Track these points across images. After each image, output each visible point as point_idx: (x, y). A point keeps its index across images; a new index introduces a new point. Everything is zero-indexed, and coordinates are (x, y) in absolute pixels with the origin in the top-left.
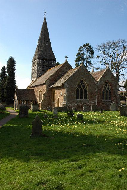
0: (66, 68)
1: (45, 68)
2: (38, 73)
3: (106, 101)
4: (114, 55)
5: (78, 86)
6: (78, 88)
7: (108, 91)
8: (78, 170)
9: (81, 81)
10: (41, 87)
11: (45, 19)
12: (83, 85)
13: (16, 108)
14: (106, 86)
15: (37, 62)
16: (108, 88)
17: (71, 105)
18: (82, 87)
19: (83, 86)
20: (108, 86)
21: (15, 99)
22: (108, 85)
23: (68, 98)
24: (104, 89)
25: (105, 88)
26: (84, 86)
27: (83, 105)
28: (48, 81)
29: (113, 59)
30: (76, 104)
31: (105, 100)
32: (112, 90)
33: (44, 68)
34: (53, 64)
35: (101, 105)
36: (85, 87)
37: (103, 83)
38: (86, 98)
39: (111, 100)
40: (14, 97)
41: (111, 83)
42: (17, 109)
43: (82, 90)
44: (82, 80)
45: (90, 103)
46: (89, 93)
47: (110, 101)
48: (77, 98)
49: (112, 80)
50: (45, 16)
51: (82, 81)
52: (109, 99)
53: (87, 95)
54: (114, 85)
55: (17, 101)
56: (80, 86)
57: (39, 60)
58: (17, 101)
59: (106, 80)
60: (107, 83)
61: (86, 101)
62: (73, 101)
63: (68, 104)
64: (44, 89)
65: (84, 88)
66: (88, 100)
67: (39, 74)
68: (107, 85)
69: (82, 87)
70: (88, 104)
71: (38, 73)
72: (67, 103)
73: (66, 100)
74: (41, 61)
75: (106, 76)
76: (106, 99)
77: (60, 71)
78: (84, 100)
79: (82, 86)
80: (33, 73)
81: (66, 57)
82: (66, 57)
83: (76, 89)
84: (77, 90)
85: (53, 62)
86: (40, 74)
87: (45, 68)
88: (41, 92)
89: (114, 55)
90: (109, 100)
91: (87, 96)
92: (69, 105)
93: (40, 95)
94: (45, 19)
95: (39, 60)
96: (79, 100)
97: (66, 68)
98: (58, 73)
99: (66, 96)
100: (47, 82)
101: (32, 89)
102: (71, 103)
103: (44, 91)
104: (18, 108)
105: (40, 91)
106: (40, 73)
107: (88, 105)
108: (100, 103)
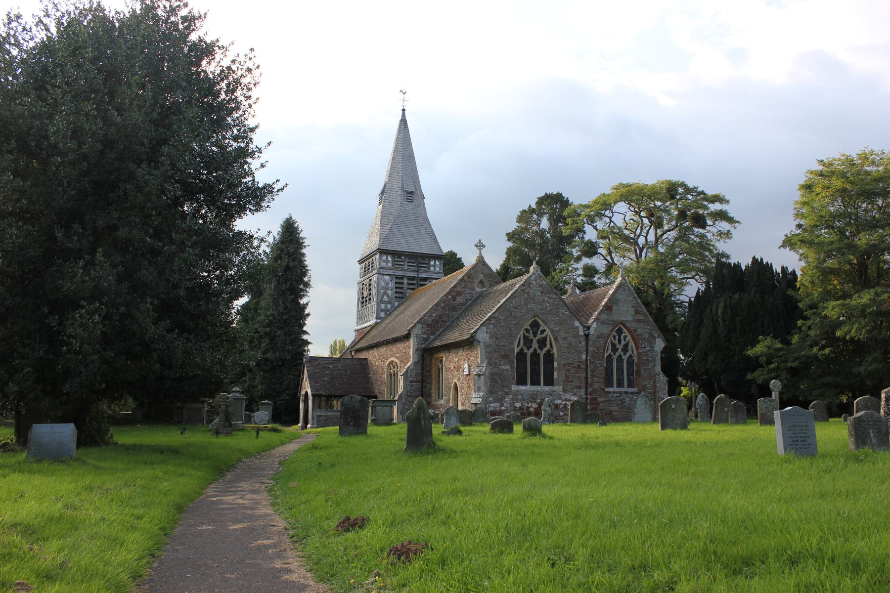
0: (481, 282)
1: (405, 286)
2: (380, 301)
3: (620, 393)
4: (646, 238)
5: (522, 342)
6: (522, 350)
7: (625, 358)
8: (785, 465)
9: (531, 325)
10: (394, 348)
11: (404, 122)
12: (539, 336)
13: (306, 422)
14: (617, 342)
15: (376, 264)
16: (625, 349)
17: (502, 405)
18: (535, 345)
19: (538, 341)
20: (623, 342)
21: (303, 393)
22: (625, 337)
23: (495, 383)
24: (610, 351)
25: (614, 349)
26: (542, 343)
27: (540, 405)
28: (419, 325)
29: (641, 251)
30: (518, 405)
31: (615, 389)
32: (639, 354)
33: (398, 285)
34: (432, 268)
35: (601, 406)
36: (546, 346)
37: (606, 330)
38: (549, 381)
39: (635, 390)
40: (298, 385)
41: (635, 331)
42: (309, 426)
43: (535, 355)
44: (535, 321)
45: (566, 400)
46: (558, 365)
47: (632, 393)
48: (521, 381)
49: (639, 321)
50: (404, 110)
51: (535, 325)
52: (630, 386)
53: (555, 373)
54: (646, 336)
55: (310, 397)
56: (528, 342)
57: (384, 258)
58: (310, 397)
59: (615, 318)
60: (620, 332)
61: (551, 394)
62: (507, 394)
63: (491, 402)
64: (405, 356)
65: (542, 350)
66: (558, 388)
67: (383, 306)
68: (622, 338)
69: (535, 345)
70: (559, 402)
71: (382, 302)
72: (485, 400)
73: (482, 388)
74: (390, 259)
75: (614, 308)
76: (620, 384)
77: (460, 294)
78: (542, 388)
79: (535, 341)
80: (364, 301)
81: (480, 246)
82: (480, 246)
83: (517, 350)
84: (521, 355)
85: (432, 263)
86: (389, 306)
87: (405, 286)
88: (395, 364)
89: (646, 238)
90: (630, 390)
91: (555, 377)
92: (492, 405)
93: (393, 376)
94: (404, 122)
95: (384, 258)
96: (528, 388)
97: (481, 282)
98: (454, 298)
99: (482, 377)
100: (415, 332)
101: (362, 356)
102: (500, 400)
103: (404, 361)
104: (313, 424)
105: (391, 363)
106: (389, 303)
107: (557, 406)
108: (600, 400)
